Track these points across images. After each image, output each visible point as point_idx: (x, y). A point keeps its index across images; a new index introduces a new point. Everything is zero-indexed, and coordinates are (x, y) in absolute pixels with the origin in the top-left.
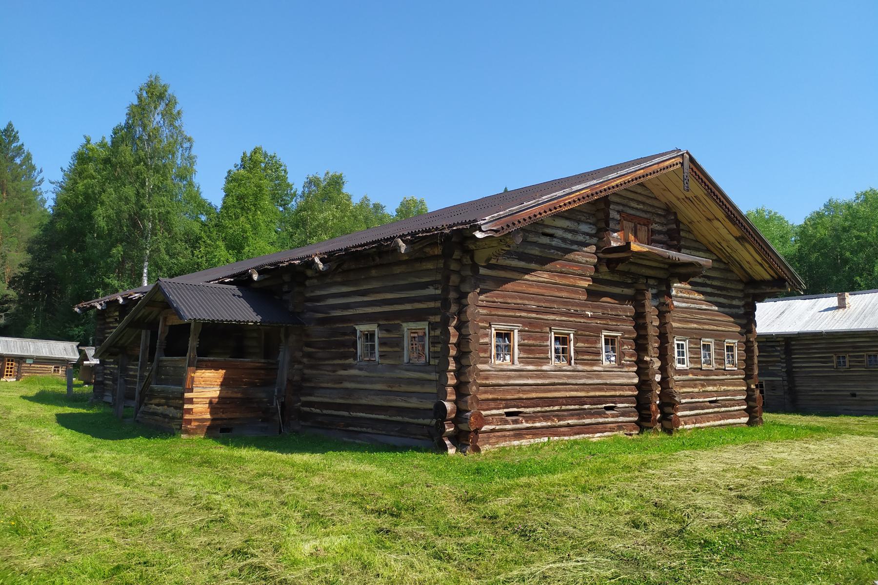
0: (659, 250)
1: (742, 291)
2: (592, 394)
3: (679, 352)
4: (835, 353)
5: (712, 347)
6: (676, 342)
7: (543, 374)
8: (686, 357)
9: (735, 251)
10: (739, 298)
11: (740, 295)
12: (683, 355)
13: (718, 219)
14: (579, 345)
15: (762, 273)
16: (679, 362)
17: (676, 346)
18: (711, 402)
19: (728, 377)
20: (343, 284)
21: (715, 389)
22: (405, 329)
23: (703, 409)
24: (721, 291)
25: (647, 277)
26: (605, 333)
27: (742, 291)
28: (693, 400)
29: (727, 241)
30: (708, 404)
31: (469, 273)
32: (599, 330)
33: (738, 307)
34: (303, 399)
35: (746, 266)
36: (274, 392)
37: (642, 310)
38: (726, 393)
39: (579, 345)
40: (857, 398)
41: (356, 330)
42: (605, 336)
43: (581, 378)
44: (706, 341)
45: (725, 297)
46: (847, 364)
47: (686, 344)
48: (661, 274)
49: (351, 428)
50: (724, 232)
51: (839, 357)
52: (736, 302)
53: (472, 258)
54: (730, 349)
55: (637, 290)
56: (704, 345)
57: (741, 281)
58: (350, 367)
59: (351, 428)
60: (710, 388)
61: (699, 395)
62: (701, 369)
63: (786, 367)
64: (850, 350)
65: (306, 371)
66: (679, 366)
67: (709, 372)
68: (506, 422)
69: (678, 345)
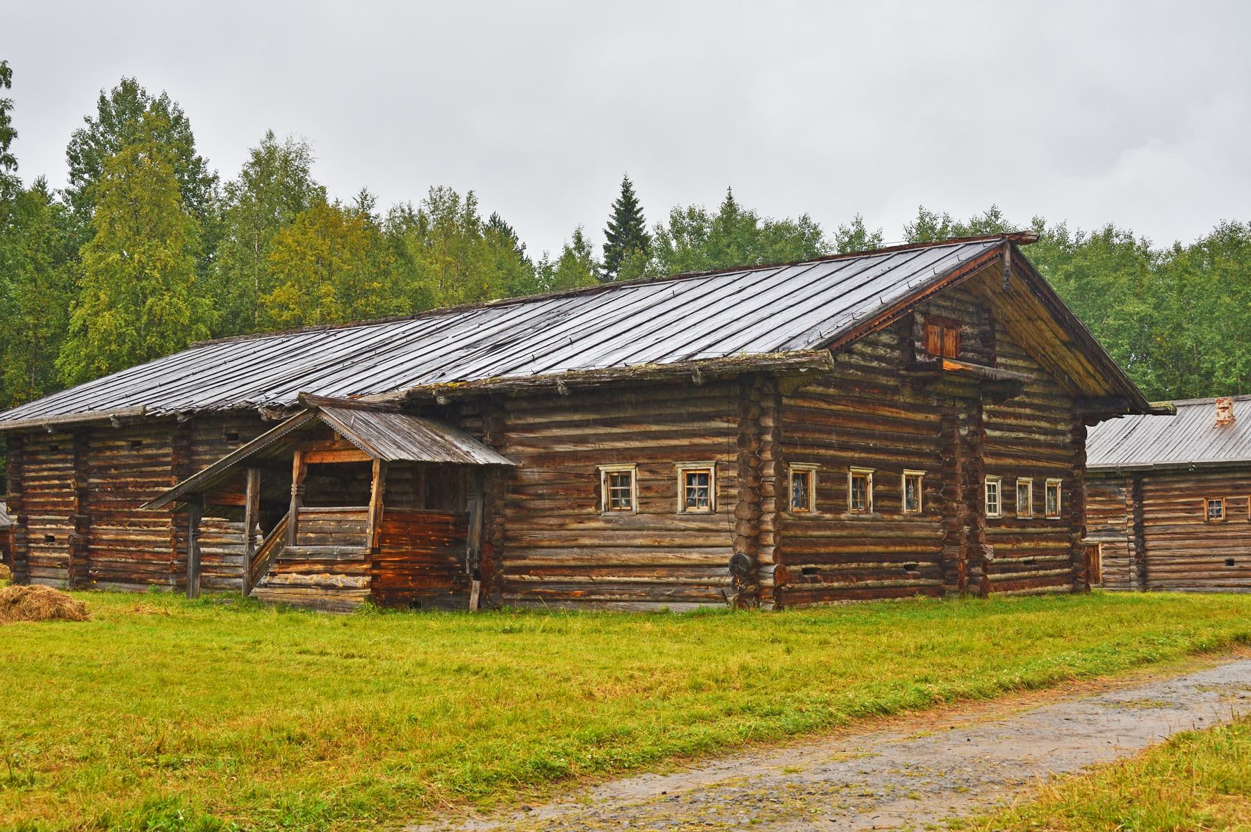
0: (972, 366)
1: (1069, 410)
2: (892, 549)
3: (989, 496)
4: (1207, 496)
5: (691, 466)
6: (986, 483)
7: (842, 525)
8: (999, 503)
9: (1063, 358)
10: (1064, 420)
11: (1066, 416)
12: (995, 501)
13: (1042, 320)
14: (880, 488)
15: (1096, 386)
16: (990, 511)
17: (986, 488)
18: (1026, 562)
19: (1049, 529)
20: (657, 422)
21: (1033, 545)
22: (680, 470)
23: (1016, 571)
24: (1043, 411)
25: (954, 398)
26: (907, 472)
27: (1069, 410)
28: (1006, 560)
29: (1053, 346)
30: (1023, 565)
31: (771, 404)
32: (899, 468)
33: (1063, 433)
34: (508, 563)
35: (1075, 377)
36: (465, 554)
37: (1037, 503)
38: (1045, 551)
39: (880, 488)
40: (1236, 566)
41: (600, 471)
42: (853, 473)
43: (880, 529)
44: (1022, 480)
45: (1047, 420)
46: (1223, 513)
47: (999, 486)
48: (968, 393)
49: (593, 597)
50: (1049, 335)
51: (1211, 503)
52: (1061, 427)
53: (776, 387)
54: (1052, 489)
55: (944, 415)
56: (1020, 486)
57: (1068, 396)
58: (590, 517)
59: (593, 597)
60: (1026, 544)
61: (1012, 553)
62: (1015, 518)
63: (1134, 519)
64: (1228, 490)
65: (508, 526)
66: (989, 515)
67: (1024, 523)
68: (805, 581)
69: (989, 486)
